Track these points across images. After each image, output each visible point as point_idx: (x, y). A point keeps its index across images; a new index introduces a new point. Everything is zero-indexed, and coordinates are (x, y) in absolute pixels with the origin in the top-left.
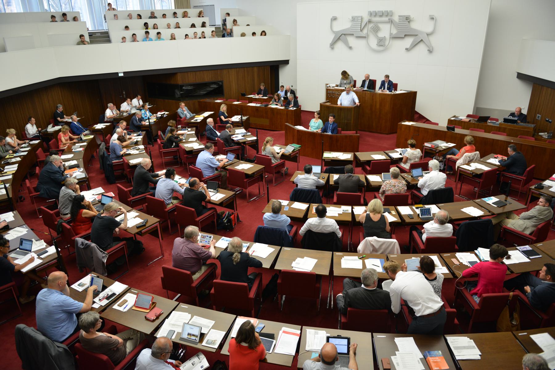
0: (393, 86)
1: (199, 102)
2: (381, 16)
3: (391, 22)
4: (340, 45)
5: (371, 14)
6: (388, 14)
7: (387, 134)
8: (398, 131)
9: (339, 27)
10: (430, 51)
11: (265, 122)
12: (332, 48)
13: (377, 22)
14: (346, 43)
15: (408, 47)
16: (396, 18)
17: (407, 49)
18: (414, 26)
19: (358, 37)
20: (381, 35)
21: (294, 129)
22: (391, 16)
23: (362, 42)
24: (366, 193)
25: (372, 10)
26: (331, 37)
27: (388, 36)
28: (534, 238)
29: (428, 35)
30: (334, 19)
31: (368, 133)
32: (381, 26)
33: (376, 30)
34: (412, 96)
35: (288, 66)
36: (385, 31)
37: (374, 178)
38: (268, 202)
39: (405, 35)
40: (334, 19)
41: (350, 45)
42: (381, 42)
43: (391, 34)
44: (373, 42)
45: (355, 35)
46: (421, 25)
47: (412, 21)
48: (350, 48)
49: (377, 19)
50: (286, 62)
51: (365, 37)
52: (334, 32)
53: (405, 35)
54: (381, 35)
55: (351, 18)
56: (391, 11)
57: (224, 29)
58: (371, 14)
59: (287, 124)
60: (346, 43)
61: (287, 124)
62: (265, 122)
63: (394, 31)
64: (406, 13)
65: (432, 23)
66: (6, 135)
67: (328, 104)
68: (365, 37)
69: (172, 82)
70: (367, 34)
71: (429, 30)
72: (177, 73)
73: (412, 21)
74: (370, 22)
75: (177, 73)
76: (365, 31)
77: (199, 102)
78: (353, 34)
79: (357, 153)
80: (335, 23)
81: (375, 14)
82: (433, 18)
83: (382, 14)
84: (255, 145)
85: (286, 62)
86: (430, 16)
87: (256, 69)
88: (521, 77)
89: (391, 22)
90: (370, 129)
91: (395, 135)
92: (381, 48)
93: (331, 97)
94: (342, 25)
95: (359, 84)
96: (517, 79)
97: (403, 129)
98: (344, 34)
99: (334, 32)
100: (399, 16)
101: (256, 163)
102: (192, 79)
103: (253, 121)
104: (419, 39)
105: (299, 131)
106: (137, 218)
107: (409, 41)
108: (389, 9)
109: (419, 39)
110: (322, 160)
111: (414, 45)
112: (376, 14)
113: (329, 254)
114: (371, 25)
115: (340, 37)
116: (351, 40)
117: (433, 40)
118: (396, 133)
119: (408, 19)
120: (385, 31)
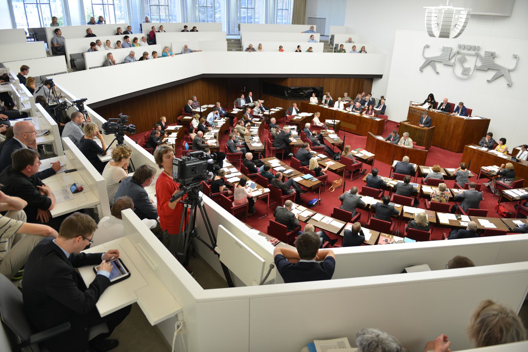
0: (467, 112)
1: (302, 103)
2: (469, 50)
3: (477, 55)
4: (429, 69)
5: (460, 47)
6: (475, 48)
7: (457, 152)
8: (464, 151)
10: (509, 86)
11: (353, 127)
14: (434, 68)
15: (490, 79)
16: (482, 53)
17: (488, 81)
18: (497, 61)
20: (466, 65)
21: (374, 138)
22: (479, 50)
23: (450, 69)
26: (422, 62)
27: (472, 68)
30: (427, 47)
31: (439, 149)
32: (468, 58)
33: (463, 61)
34: (486, 123)
36: (471, 62)
37: (427, 189)
38: (344, 192)
39: (488, 69)
40: (427, 47)
41: (438, 71)
42: (466, 72)
43: (475, 66)
44: (459, 70)
46: (504, 61)
47: (497, 57)
48: (438, 73)
50: (380, 77)
52: (425, 58)
54: (466, 65)
55: (442, 48)
56: (479, 47)
57: (331, 43)
58: (460, 47)
59: (370, 133)
60: (434, 68)
61: (370, 133)
62: (353, 127)
63: (479, 64)
65: (515, 61)
67: (406, 123)
69: (283, 84)
70: (454, 63)
71: (511, 67)
72: (287, 78)
74: (458, 53)
75: (287, 78)
76: (453, 61)
77: (302, 103)
79: (421, 167)
80: (427, 50)
82: (516, 58)
83: (471, 48)
84: (341, 147)
85: (380, 77)
86: (514, 55)
87: (352, 80)
89: (477, 55)
90: (442, 146)
91: (462, 154)
92: (465, 77)
93: (413, 114)
97: (468, 151)
99: (425, 58)
100: (485, 52)
101: (340, 162)
102: (299, 84)
103: (344, 124)
104: (500, 73)
105: (378, 141)
107: (491, 74)
108: (477, 45)
109: (500, 73)
111: (495, 78)
112: (465, 47)
113: (378, 233)
114: (459, 56)
115: (430, 62)
116: (439, 67)
118: (462, 152)
119: (493, 55)
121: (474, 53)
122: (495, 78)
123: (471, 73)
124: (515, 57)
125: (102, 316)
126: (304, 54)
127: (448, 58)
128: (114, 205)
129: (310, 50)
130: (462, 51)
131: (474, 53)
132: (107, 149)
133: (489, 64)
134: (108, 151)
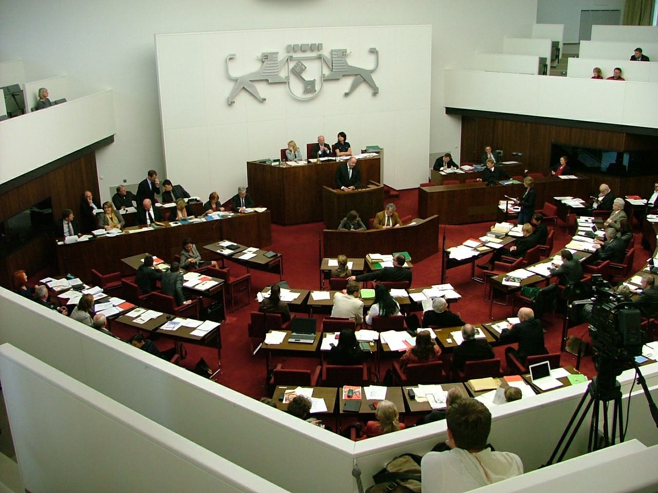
2: (304, 51)
3: (320, 57)
5: (293, 49)
6: (319, 47)
9: (237, 71)
12: (264, 100)
15: (347, 91)
16: (326, 53)
18: (352, 62)
20: (307, 76)
23: (280, 89)
24: (313, 315)
28: (526, 262)
29: (372, 71)
32: (305, 64)
33: (298, 72)
41: (262, 96)
42: (309, 87)
44: (297, 88)
46: (360, 60)
47: (259, 60)
48: (231, 103)
49: (299, 55)
51: (285, 83)
54: (307, 76)
65: (372, 58)
66: (595, 288)
68: (285, 83)
70: (288, 78)
73: (259, 60)
74: (290, 59)
80: (230, 64)
83: (303, 49)
88: (450, 111)
89: (320, 57)
92: (309, 96)
94: (247, 67)
96: (446, 115)
106: (544, 389)
107: (347, 83)
109: (363, 78)
110: (320, 270)
111: (354, 87)
115: (245, 86)
116: (262, 89)
119: (343, 53)
120: (313, 71)
121: (314, 54)
122: (354, 87)
123: (317, 88)
124: (373, 51)
125: (368, 399)
126: (604, 84)
127: (269, 73)
128: (288, 409)
129: (618, 76)
130: (295, 55)
131: (314, 54)
132: (508, 322)
133: (339, 67)
134: (507, 323)
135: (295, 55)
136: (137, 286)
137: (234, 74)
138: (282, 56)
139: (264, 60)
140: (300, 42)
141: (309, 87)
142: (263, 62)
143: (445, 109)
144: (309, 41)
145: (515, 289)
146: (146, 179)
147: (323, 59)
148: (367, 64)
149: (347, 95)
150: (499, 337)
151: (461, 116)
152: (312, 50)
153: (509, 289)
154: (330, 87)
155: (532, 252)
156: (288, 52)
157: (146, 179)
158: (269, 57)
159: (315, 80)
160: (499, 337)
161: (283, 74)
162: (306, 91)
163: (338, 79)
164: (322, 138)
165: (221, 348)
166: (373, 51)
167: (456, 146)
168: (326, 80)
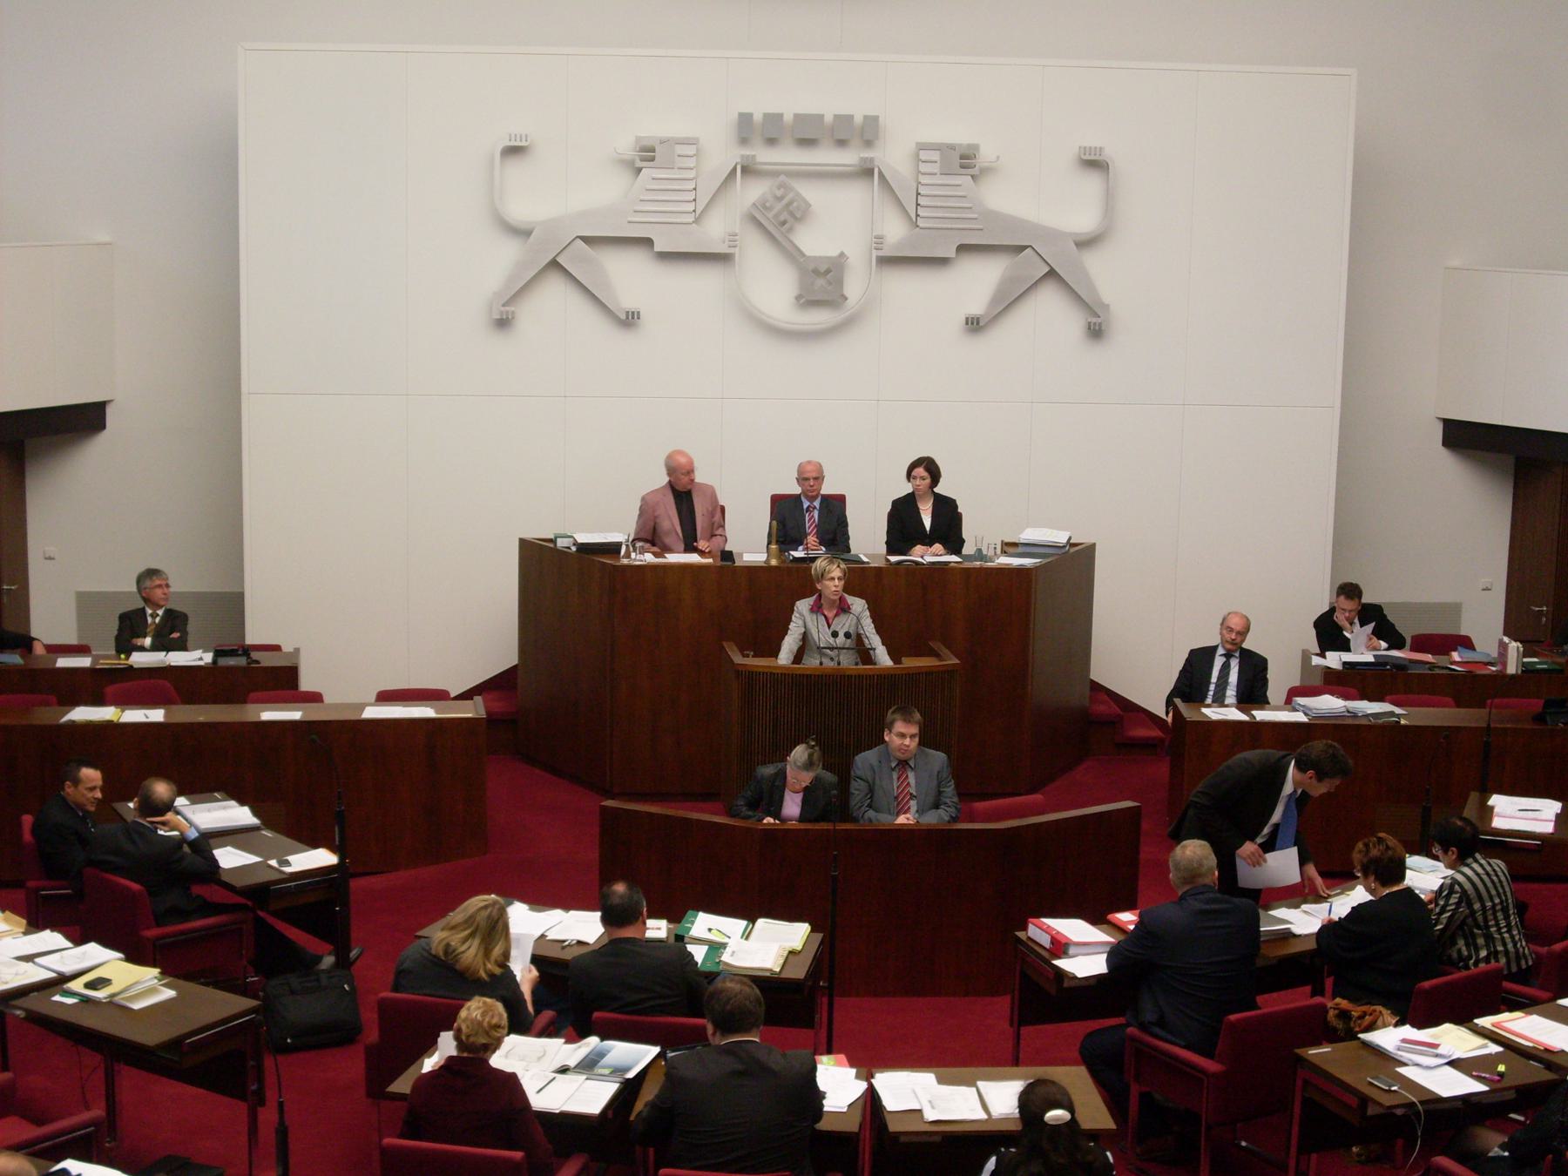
2: (807, 143)
5: (746, 129)
6: (868, 132)
9: (539, 198)
13: (789, 174)
15: (977, 308)
16: (894, 156)
19: (666, 256)
23: (703, 280)
25: (758, 109)
29: (1086, 243)
32: (811, 193)
33: (778, 223)
35: (103, 439)
39: (963, 248)
42: (821, 285)
44: (771, 285)
45: (657, 248)
46: (1036, 194)
48: (503, 323)
49: (788, 156)
53: (963, 248)
54: (814, 242)
58: (746, 129)
63: (895, 231)
64: (959, 136)
65: (1092, 184)
71: (1083, 220)
78: (647, 242)
80: (516, 170)
81: (770, 131)
83: (807, 133)
85: (84, 420)
88: (1464, 437)
92: (820, 318)
94: (574, 190)
95: (868, 537)
96: (1444, 454)
98: (586, 239)
104: (1040, 268)
107: (977, 282)
109: (1040, 268)
111: (1007, 302)
114: (752, 192)
116: (628, 277)
117: (1104, 274)
119: (965, 160)
120: (840, 223)
121: (849, 158)
122: (1007, 302)
123: (854, 288)
124: (1094, 164)
130: (765, 156)
131: (849, 158)
135: (765, 156)
136: (136, 886)
137: (521, 210)
138: (721, 154)
139: (639, 164)
140: (790, 105)
141: (821, 285)
142: (639, 170)
143: (1439, 428)
144: (828, 105)
145: (1388, 1115)
146: (1214, 649)
147: (880, 173)
148: (1070, 209)
149: (974, 325)
150: (481, 1055)
151: (1511, 460)
152: (842, 143)
153: (1371, 1111)
154: (907, 287)
155: (1435, 988)
156: (744, 141)
157: (1214, 649)
158: (657, 154)
159: (842, 255)
160: (481, 1055)
161: (715, 232)
162: (808, 301)
163: (942, 262)
164: (683, 460)
165: (261, 1101)
166: (1094, 164)
167: (1484, 581)
168: (890, 261)
